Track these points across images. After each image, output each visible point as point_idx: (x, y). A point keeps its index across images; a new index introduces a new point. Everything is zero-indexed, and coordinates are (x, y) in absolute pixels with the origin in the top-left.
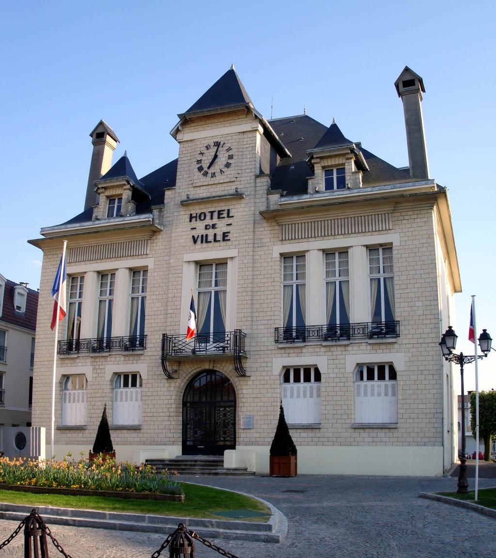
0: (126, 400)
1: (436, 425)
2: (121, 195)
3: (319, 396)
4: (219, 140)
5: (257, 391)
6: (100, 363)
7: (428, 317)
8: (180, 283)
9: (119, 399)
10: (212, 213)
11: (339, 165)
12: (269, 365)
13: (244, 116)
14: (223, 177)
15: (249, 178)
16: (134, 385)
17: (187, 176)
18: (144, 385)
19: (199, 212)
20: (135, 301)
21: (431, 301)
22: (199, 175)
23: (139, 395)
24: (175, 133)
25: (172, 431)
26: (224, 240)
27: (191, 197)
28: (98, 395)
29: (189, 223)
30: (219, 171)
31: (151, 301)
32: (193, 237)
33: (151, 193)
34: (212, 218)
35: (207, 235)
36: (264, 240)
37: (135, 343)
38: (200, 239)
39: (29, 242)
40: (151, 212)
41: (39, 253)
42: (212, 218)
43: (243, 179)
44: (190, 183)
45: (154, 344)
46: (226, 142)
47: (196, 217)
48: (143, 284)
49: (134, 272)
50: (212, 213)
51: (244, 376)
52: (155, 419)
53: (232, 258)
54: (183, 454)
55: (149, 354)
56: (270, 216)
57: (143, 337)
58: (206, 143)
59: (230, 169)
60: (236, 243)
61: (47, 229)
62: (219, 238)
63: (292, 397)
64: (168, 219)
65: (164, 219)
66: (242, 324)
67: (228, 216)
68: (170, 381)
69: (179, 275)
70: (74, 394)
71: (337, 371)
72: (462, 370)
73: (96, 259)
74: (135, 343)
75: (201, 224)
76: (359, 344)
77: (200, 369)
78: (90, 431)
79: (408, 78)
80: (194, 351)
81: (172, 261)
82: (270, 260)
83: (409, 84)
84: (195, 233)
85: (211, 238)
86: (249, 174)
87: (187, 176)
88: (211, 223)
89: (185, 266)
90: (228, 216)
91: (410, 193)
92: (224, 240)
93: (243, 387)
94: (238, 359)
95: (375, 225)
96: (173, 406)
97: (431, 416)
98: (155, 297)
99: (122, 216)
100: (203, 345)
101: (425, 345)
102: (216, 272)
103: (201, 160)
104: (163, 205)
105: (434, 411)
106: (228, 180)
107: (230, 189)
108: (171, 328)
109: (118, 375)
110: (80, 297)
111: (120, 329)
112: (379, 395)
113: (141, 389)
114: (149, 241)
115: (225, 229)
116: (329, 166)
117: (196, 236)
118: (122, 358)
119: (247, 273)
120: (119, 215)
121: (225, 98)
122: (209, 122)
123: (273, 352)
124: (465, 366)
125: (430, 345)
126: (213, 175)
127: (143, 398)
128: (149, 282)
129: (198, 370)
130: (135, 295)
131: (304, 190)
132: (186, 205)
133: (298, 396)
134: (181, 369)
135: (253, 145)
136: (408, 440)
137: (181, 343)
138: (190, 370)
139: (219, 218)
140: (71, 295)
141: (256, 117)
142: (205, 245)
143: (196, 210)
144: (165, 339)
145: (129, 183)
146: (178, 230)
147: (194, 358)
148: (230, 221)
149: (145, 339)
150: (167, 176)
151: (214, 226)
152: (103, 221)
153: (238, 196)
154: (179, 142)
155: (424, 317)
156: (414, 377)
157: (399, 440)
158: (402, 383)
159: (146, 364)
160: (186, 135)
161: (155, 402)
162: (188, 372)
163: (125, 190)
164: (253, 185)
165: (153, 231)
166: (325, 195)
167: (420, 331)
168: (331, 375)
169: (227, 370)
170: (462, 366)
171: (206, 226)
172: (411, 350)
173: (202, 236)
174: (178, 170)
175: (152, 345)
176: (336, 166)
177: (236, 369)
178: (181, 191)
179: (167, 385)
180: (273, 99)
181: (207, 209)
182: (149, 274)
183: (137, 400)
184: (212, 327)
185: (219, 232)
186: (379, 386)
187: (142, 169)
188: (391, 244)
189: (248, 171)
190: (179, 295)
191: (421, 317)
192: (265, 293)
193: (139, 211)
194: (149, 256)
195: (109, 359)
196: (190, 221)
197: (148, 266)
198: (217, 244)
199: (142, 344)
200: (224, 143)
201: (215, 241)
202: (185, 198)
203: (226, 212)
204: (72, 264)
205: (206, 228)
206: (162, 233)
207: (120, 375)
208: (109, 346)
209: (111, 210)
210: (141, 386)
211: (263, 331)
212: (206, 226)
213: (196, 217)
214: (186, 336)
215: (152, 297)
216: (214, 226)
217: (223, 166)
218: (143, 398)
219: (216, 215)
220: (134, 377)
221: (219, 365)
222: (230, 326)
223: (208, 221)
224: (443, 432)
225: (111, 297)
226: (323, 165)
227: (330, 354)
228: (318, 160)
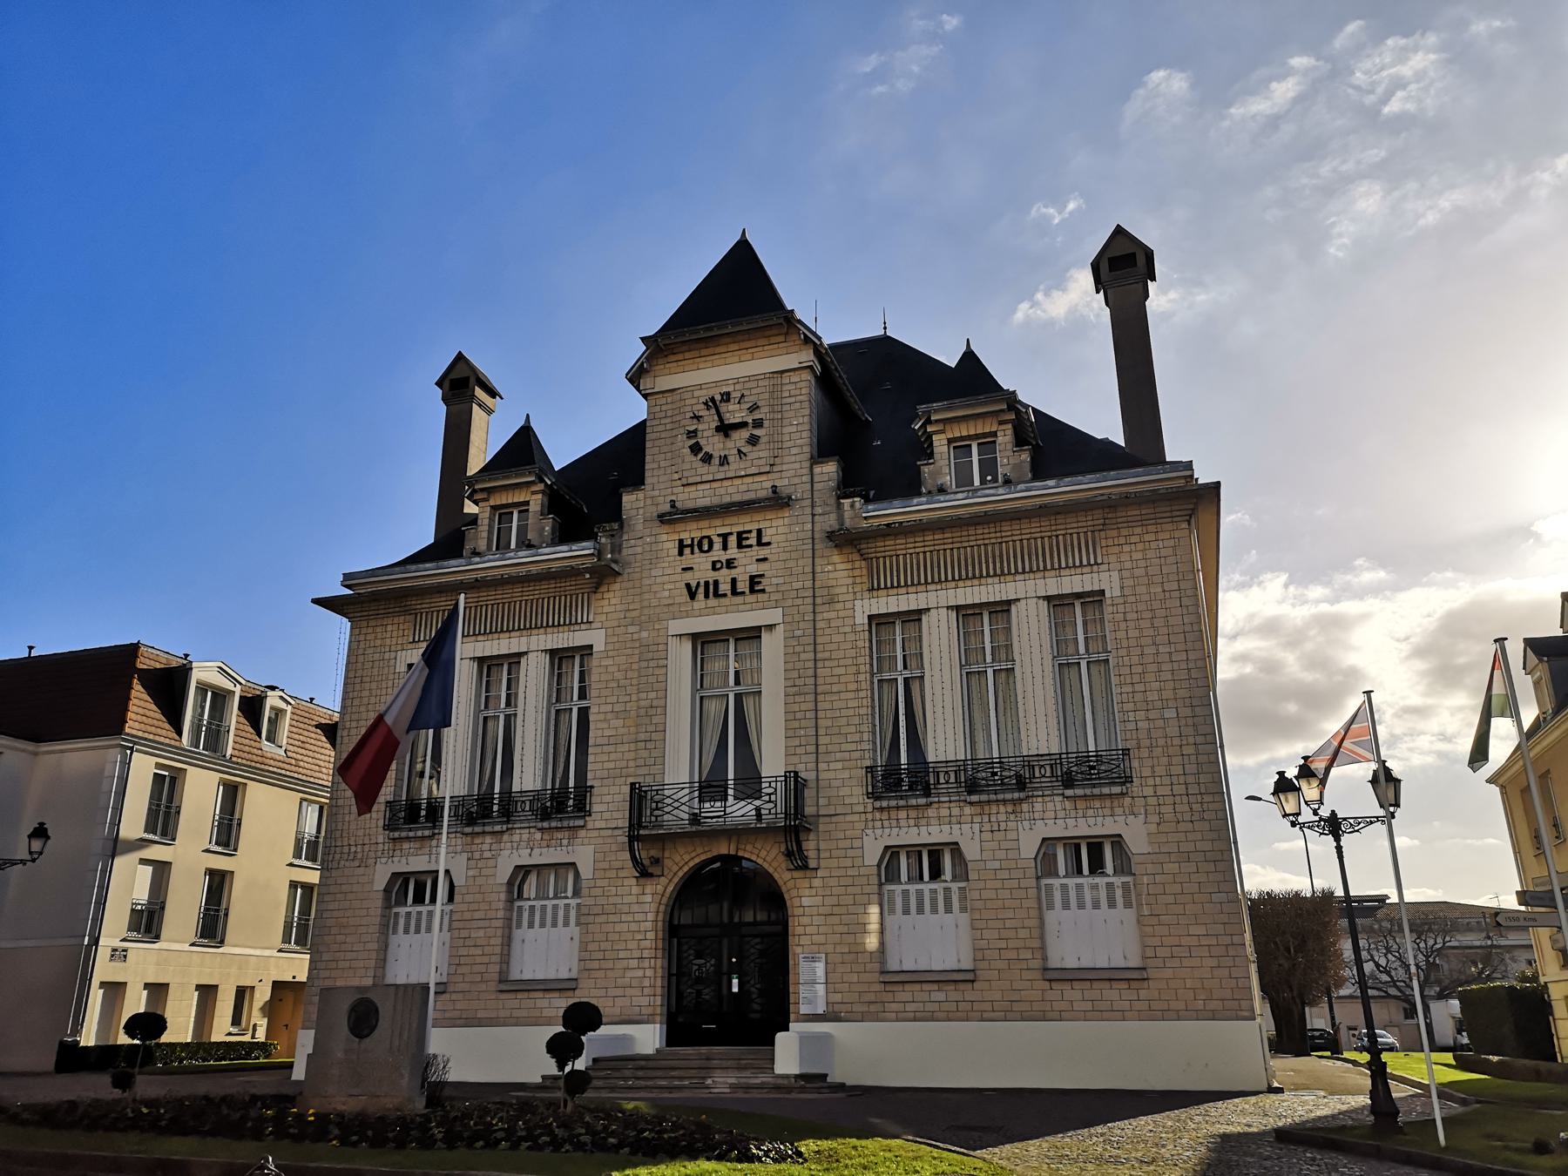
0: (543, 925)
2: (527, 503)
5: (834, 900)
9: (525, 923)
10: (725, 537)
11: (984, 435)
13: (782, 338)
15: (797, 466)
17: (668, 463)
18: (457, 898)
19: (697, 535)
20: (564, 718)
22: (695, 461)
23: (573, 914)
25: (646, 991)
26: (752, 591)
28: (477, 915)
31: (602, 717)
32: (688, 586)
33: (592, 496)
34: (725, 548)
35: (716, 583)
37: (564, 805)
38: (701, 590)
39: (316, 601)
40: (592, 536)
42: (725, 548)
43: (785, 467)
44: (676, 476)
45: (610, 804)
47: (692, 546)
49: (559, 657)
50: (725, 537)
51: (805, 867)
52: (610, 964)
53: (771, 627)
54: (668, 1045)
55: (598, 824)
56: (844, 540)
57: (583, 790)
60: (778, 596)
62: (743, 586)
64: (630, 551)
65: (625, 552)
66: (795, 759)
67: (760, 543)
68: (642, 881)
69: (662, 662)
71: (1001, 855)
72: (1339, 849)
74: (564, 805)
77: (709, 855)
78: (454, 997)
79: (1121, 249)
80: (695, 819)
82: (848, 629)
83: (1124, 268)
85: (725, 587)
86: (798, 458)
87: (668, 463)
88: (723, 557)
90: (760, 543)
91: (1135, 494)
92: (752, 591)
93: (801, 892)
94: (794, 830)
96: (651, 935)
98: (609, 708)
99: (530, 546)
100: (718, 804)
103: (695, 431)
104: (616, 526)
106: (754, 470)
107: (760, 488)
108: (644, 771)
111: (529, 776)
112: (1096, 905)
114: (593, 597)
115: (754, 569)
116: (962, 438)
117: (694, 584)
118: (538, 836)
119: (803, 656)
120: (525, 544)
121: (736, 298)
124: (1346, 840)
127: (583, 920)
128: (594, 677)
129: (703, 857)
131: (911, 487)
132: (670, 522)
133: (920, 910)
134: (667, 854)
137: (668, 801)
138: (687, 858)
139: (740, 546)
140: (1469, 929)
141: (807, 340)
142: (712, 602)
143: (691, 532)
144: (639, 797)
145: (542, 481)
147: (697, 831)
148: (763, 552)
150: (622, 460)
151: (730, 564)
153: (778, 501)
154: (645, 396)
159: (593, 848)
161: (609, 928)
162: (680, 862)
163: (534, 493)
164: (806, 479)
165: (602, 575)
166: (960, 496)
168: (990, 865)
169: (767, 857)
170: (1337, 840)
171: (714, 563)
174: (648, 452)
175: (603, 808)
176: (976, 437)
177: (789, 854)
178: (656, 493)
179: (635, 890)
180: (835, 306)
181: (713, 529)
182: (595, 661)
183: (566, 924)
184: (730, 763)
185: (742, 575)
187: (564, 447)
190: (662, 702)
192: (843, 696)
193: (564, 536)
195: (506, 837)
196: (681, 553)
198: (739, 599)
199: (582, 809)
201: (735, 592)
202: (667, 508)
203: (754, 534)
205: (714, 569)
206: (619, 579)
208: (507, 813)
212: (714, 563)
213: (692, 546)
215: (603, 708)
216: (730, 564)
217: (743, 443)
218: (583, 920)
219: (733, 540)
221: (749, 847)
222: (772, 764)
223: (718, 554)
226: (492, 503)
228: (940, 427)
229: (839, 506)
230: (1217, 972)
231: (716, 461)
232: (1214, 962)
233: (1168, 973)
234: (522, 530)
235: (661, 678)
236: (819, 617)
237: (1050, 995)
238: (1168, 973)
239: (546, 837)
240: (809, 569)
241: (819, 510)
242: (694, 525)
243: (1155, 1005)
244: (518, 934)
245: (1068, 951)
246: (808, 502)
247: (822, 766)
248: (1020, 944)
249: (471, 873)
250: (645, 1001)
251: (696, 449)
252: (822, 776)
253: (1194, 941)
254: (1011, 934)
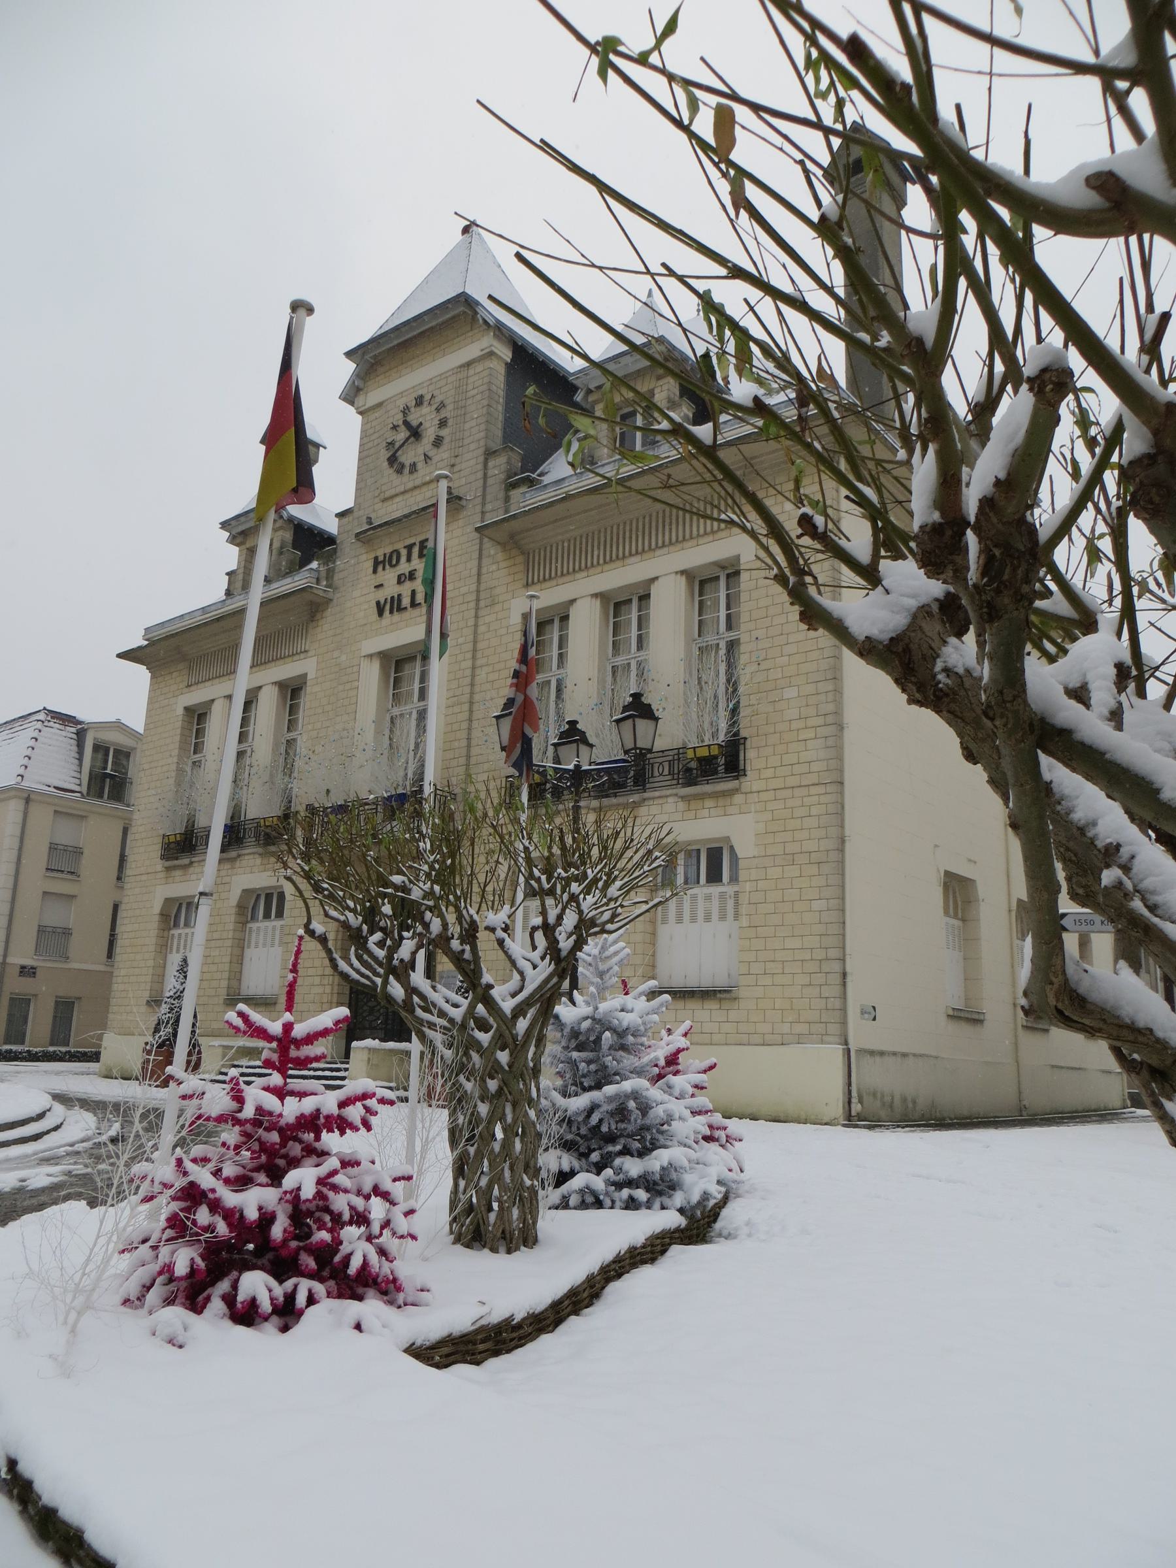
1: (826, 991)
3: (737, 916)
4: (420, 393)
7: (811, 722)
8: (353, 700)
10: (410, 548)
16: (714, 876)
18: (743, 875)
19: (388, 550)
21: (820, 684)
29: (373, 576)
34: (409, 560)
35: (399, 596)
36: (497, 591)
38: (388, 607)
41: (140, 674)
47: (383, 562)
48: (728, 608)
50: (410, 548)
58: (400, 404)
59: (441, 450)
61: (213, 608)
63: (679, 920)
70: (180, 935)
73: (681, 538)
75: (392, 575)
76: (661, 801)
81: (344, 658)
82: (503, 631)
84: (382, 595)
85: (406, 601)
89: (365, 663)
95: (657, 535)
97: (812, 967)
101: (804, 791)
102: (728, 595)
105: (820, 954)
113: (736, 888)
125: (813, 790)
126: (413, 468)
130: (620, 660)
135: (366, 440)
142: (397, 616)
146: (357, 593)
149: (742, 747)
154: (361, 413)
155: (801, 724)
156: (774, 872)
158: (748, 887)
160: (373, 397)
167: (793, 758)
172: (770, 806)
173: (392, 598)
186: (708, 898)
188: (737, 558)
189: (472, 447)
191: (794, 725)
194: (310, 654)
204: (192, 688)
212: (399, 577)
214: (1157, 674)
220: (715, 856)
223: (404, 567)
224: (844, 1010)
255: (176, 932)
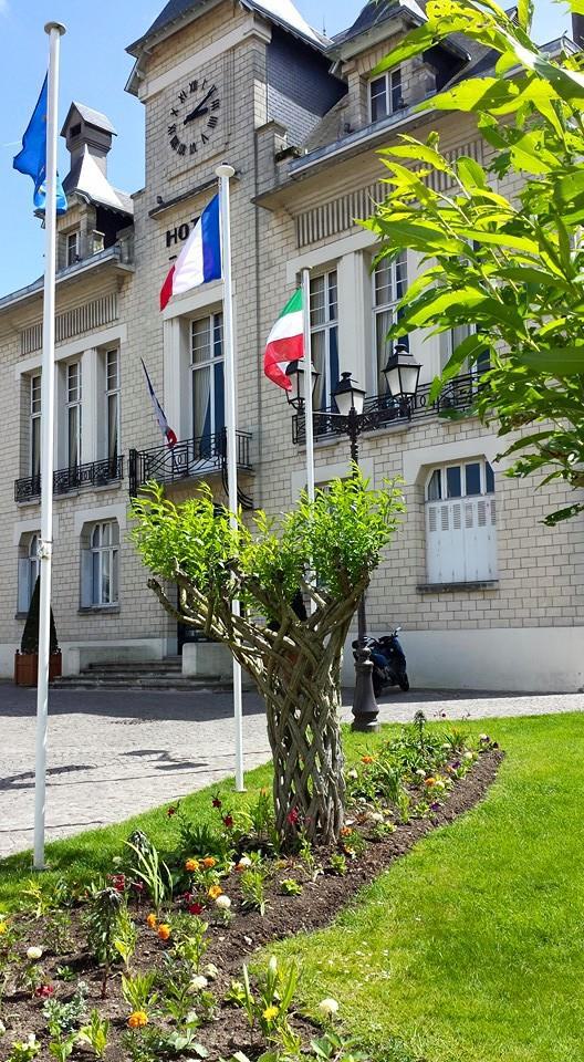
4: (194, 79)
6: (392, 449)
12: (287, 484)
14: (207, 148)
16: (473, 489)
18: (497, 486)
19: (178, 225)
24: (133, 89)
27: (165, 200)
30: (200, 138)
46: (208, 78)
47: (175, 236)
58: (178, 90)
63: (445, 527)
65: (136, 252)
89: (167, 326)
106: (214, 152)
109: (431, 472)
110: (332, 317)
112: (469, 524)
113: (492, 497)
122: (179, 47)
123: (293, 461)
136: (520, 613)
152: (362, 134)
154: (144, 102)
157: (503, 614)
158: (503, 496)
163: (82, 214)
166: (395, 119)
197: (119, 339)
200: (205, 81)
207: (439, 471)
209: (377, 104)
210: (491, 488)
211: (276, 425)
220: (473, 472)
225: (35, 415)
226: (361, 72)
227: (377, 452)
229: (276, 170)
230: (559, 581)
231: (188, 151)
232: (556, 571)
233: (517, 583)
234: (397, 94)
235: (160, 359)
236: (262, 283)
237: (426, 607)
238: (517, 583)
239: (100, 498)
240: (253, 238)
241: (261, 179)
242: (176, 217)
243: (503, 614)
244: (433, 538)
245: (444, 570)
246: (253, 173)
247: (264, 419)
248: (400, 563)
249: (61, 530)
250: (157, 621)
251: (175, 142)
252: (264, 428)
253: (540, 552)
254: (395, 555)
255: (438, 505)
